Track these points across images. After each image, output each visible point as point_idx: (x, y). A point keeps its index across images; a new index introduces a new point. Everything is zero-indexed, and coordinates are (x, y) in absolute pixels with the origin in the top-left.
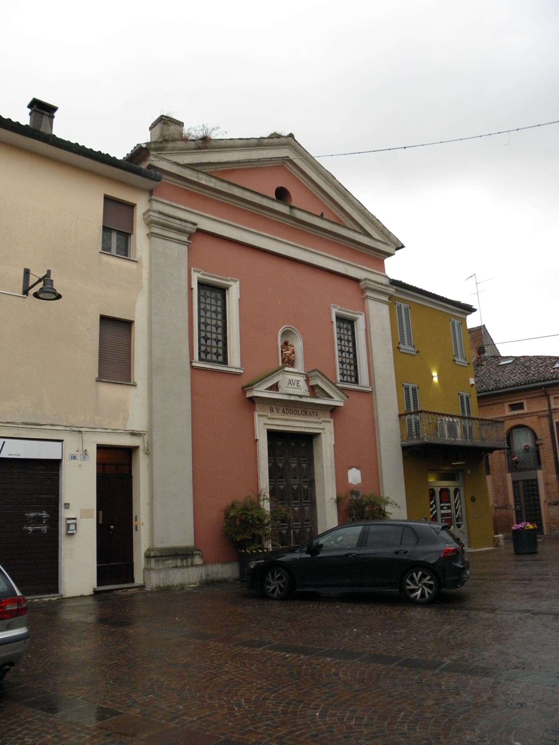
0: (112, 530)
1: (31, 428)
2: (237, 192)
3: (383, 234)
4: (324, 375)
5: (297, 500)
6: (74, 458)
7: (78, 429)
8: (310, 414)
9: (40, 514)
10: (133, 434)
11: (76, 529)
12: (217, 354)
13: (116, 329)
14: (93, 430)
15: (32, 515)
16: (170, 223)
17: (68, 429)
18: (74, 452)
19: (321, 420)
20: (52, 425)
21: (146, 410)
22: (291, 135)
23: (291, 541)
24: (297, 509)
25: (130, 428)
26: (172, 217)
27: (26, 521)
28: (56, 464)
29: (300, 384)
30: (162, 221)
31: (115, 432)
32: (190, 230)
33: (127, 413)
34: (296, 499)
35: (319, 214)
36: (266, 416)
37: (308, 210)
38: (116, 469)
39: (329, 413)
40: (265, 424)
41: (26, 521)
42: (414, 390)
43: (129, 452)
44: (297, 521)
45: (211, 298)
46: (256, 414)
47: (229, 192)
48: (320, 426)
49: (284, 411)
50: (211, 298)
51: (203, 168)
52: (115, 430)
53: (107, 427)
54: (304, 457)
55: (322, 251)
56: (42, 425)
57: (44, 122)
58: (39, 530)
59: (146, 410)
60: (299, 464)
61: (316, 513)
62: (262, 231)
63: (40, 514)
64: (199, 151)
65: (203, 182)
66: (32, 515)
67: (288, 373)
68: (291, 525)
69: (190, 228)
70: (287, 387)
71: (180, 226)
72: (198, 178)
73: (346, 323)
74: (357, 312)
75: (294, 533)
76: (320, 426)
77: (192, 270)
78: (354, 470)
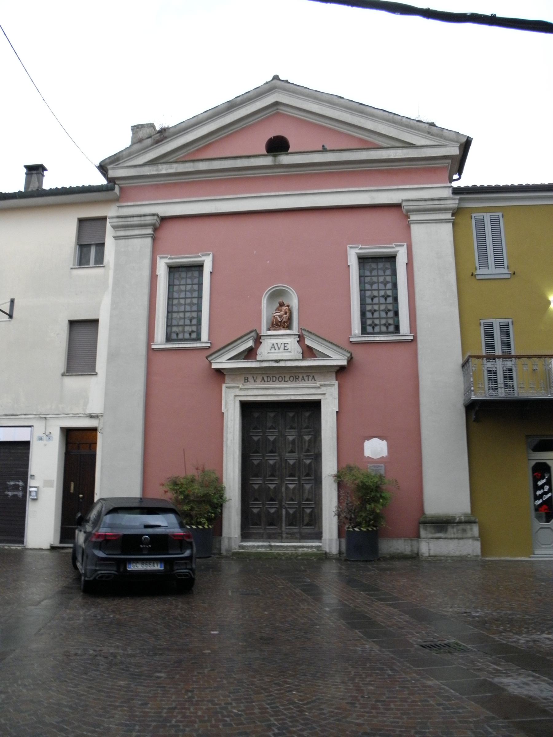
0: (82, 498)
1: (11, 418)
2: (203, 166)
3: (432, 135)
4: (311, 333)
5: (294, 476)
6: (41, 439)
7: (45, 416)
8: (263, 379)
9: (17, 483)
10: (91, 416)
11: (36, 495)
12: (387, 325)
13: (82, 329)
14: (57, 416)
15: (12, 483)
16: (129, 223)
17: (37, 416)
18: (41, 434)
19: (318, 384)
20: (25, 415)
21: (100, 394)
22: (276, 78)
23: (281, 522)
24: (291, 486)
25: (88, 411)
26: (130, 217)
27: (7, 488)
28: (27, 444)
29: (288, 346)
30: (121, 223)
31: (76, 416)
32: (150, 222)
33: (90, 399)
34: (292, 475)
35: (321, 149)
36: (238, 387)
37: (315, 149)
38: (79, 447)
39: (334, 375)
40: (236, 396)
41: (7, 488)
42: (505, 327)
43: (91, 433)
44: (292, 500)
46: (224, 386)
47: (193, 170)
49: (263, 379)
51: (170, 157)
52: (57, 414)
53: (69, 413)
54: (307, 427)
55: (331, 188)
56: (17, 415)
57: (33, 180)
58: (16, 495)
59: (100, 394)
60: (300, 436)
61: (321, 492)
62: (308, 190)
63: (17, 483)
64: (159, 144)
65: (164, 172)
66: (12, 483)
68: (284, 504)
69: (149, 220)
70: (269, 353)
71: (139, 222)
72: (157, 170)
73: (377, 265)
74: (393, 245)
75: (287, 513)
77: (348, 248)
78: (375, 441)
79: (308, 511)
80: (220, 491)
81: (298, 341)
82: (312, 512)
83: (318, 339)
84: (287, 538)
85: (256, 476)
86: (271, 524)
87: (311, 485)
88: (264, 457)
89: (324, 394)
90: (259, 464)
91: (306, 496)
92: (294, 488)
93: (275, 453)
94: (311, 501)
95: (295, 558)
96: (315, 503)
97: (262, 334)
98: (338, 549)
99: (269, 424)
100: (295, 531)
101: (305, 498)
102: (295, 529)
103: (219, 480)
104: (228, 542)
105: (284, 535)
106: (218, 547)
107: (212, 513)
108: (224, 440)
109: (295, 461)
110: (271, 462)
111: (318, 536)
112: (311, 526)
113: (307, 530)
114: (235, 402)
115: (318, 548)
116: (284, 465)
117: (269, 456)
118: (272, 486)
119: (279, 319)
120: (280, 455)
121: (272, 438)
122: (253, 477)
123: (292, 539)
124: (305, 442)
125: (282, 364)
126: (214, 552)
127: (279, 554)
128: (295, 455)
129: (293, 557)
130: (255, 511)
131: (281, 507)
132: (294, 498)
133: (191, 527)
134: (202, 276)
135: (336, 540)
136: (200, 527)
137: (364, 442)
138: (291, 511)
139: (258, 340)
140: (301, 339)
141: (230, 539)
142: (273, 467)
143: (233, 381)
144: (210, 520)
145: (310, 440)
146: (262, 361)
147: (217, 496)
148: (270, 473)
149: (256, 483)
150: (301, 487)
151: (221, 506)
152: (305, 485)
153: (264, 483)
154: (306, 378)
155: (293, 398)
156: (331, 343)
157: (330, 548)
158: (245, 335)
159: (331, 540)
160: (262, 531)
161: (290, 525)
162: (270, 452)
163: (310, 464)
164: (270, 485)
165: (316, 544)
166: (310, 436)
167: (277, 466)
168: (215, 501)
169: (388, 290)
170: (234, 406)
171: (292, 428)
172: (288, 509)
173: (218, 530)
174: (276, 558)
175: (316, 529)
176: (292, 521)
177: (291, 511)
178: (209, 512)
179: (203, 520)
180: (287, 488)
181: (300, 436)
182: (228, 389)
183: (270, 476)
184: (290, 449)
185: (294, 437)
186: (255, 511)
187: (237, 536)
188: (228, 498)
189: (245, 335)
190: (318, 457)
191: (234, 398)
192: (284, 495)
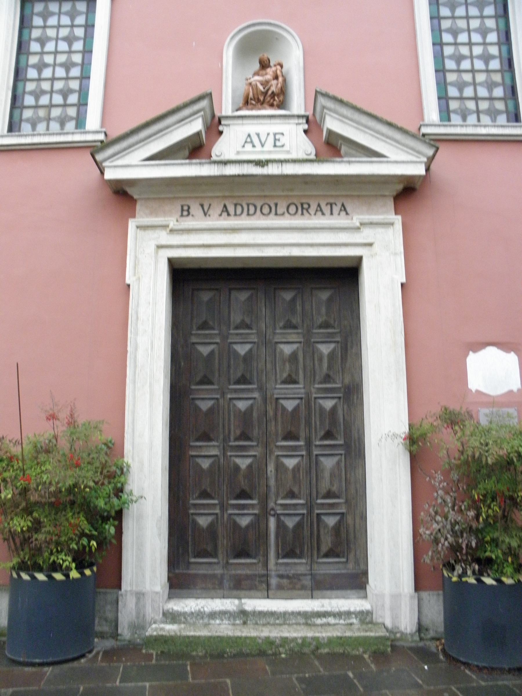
4: (341, 102)
24: (290, 463)
29: (283, 140)
34: (290, 436)
39: (392, 200)
40: (160, 247)
44: (292, 495)
45: (72, 26)
46: (132, 224)
48: (357, 238)
50: (72, 26)
54: (326, 325)
60: (309, 345)
67: (245, 121)
68: (271, 504)
75: (280, 525)
76: (357, 238)
78: (491, 353)
79: (331, 521)
80: (114, 475)
81: (305, 132)
82: (339, 522)
83: (357, 116)
84: (280, 587)
85: (206, 437)
86: (242, 552)
87: (336, 459)
88: (223, 394)
89: (370, 245)
90: (211, 410)
91: (325, 485)
92: (296, 469)
93: (250, 383)
94: (338, 497)
95: (313, 652)
96: (347, 502)
97: (224, 114)
98: (416, 620)
99: (236, 318)
100: (302, 569)
101: (323, 491)
102: (300, 566)
103: (114, 448)
104: (137, 604)
105: (274, 581)
106: (110, 615)
107: (90, 537)
108: (130, 349)
109: (296, 402)
110: (242, 405)
111: (357, 581)
112: (338, 556)
113: (328, 567)
114: (156, 262)
115: (365, 617)
116: (271, 413)
117: (236, 391)
118: (243, 463)
119: (261, 88)
120: (261, 389)
121: (242, 350)
122: (197, 440)
123: (294, 588)
124: (321, 360)
125: (273, 170)
126: (97, 628)
127: (269, 641)
128: (299, 389)
129: (306, 650)
130: (203, 522)
131: (265, 512)
132: (296, 490)
133: (33, 578)
134: (94, 12)
135: (411, 597)
136: (59, 576)
137: (467, 355)
138: (290, 523)
139: (215, 126)
140: (312, 126)
141: (140, 596)
142: (246, 417)
143: (153, 213)
144: (81, 561)
145: (332, 355)
146: (225, 163)
147: (109, 488)
148: (238, 432)
149: (206, 455)
150: (312, 465)
151: (119, 515)
152: (322, 459)
153: (224, 454)
154: (326, 210)
155: (296, 252)
156: (390, 124)
157: (395, 617)
158: (186, 106)
159: (396, 597)
160: (218, 571)
161: (285, 556)
162: (238, 382)
163: (334, 409)
164: (238, 461)
165: (352, 603)
166: (332, 346)
167: (255, 414)
168: (101, 503)
169: (491, 44)
170: (156, 268)
171: (289, 326)
172: (282, 518)
173: (111, 575)
174: (262, 653)
175: (351, 565)
176: (292, 546)
177: (290, 523)
178: (83, 534)
179: (66, 560)
180: (280, 467)
181: (309, 345)
182: (140, 233)
183: (236, 439)
184: (285, 375)
185: (295, 346)
186: (203, 522)
187: (158, 588)
188: (136, 493)
189: (186, 106)
190: (352, 393)
191: (157, 253)
192: (272, 482)
